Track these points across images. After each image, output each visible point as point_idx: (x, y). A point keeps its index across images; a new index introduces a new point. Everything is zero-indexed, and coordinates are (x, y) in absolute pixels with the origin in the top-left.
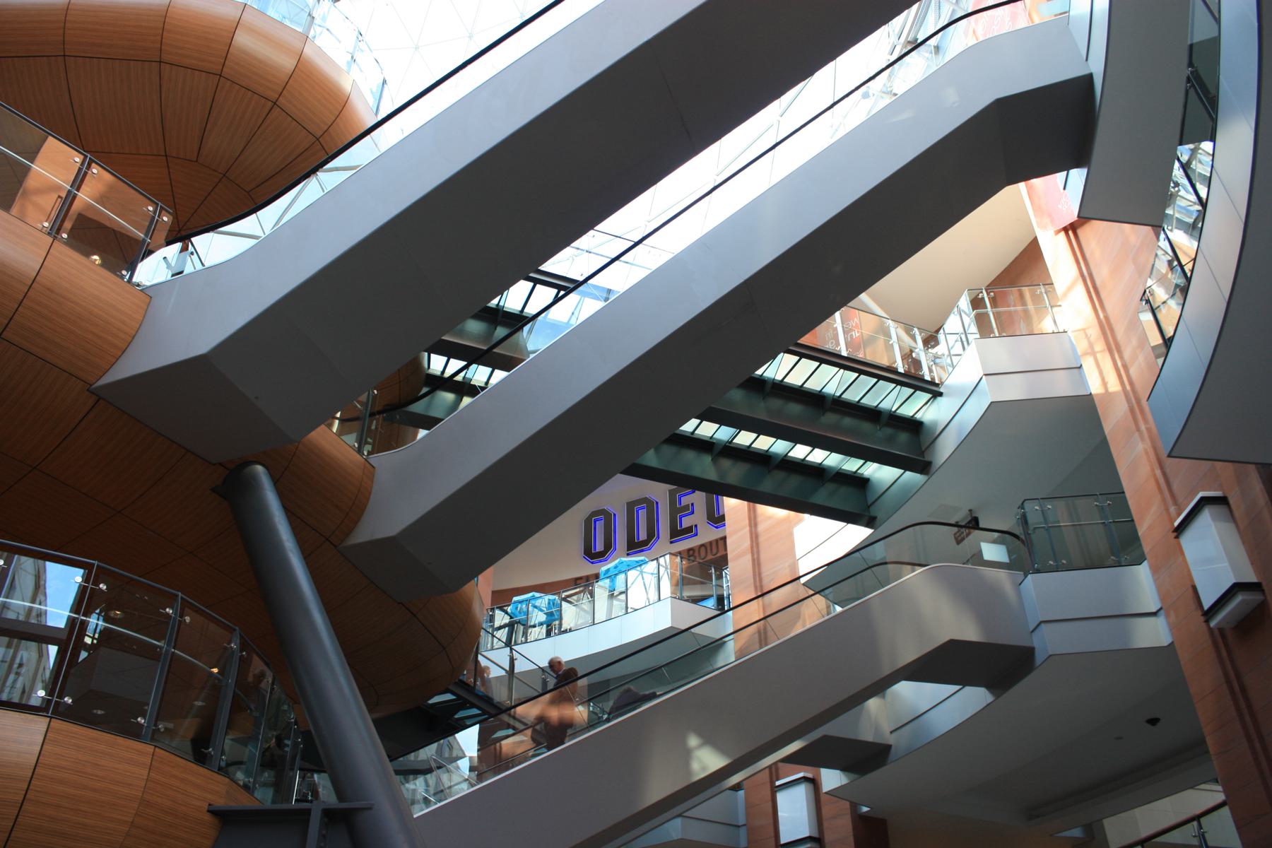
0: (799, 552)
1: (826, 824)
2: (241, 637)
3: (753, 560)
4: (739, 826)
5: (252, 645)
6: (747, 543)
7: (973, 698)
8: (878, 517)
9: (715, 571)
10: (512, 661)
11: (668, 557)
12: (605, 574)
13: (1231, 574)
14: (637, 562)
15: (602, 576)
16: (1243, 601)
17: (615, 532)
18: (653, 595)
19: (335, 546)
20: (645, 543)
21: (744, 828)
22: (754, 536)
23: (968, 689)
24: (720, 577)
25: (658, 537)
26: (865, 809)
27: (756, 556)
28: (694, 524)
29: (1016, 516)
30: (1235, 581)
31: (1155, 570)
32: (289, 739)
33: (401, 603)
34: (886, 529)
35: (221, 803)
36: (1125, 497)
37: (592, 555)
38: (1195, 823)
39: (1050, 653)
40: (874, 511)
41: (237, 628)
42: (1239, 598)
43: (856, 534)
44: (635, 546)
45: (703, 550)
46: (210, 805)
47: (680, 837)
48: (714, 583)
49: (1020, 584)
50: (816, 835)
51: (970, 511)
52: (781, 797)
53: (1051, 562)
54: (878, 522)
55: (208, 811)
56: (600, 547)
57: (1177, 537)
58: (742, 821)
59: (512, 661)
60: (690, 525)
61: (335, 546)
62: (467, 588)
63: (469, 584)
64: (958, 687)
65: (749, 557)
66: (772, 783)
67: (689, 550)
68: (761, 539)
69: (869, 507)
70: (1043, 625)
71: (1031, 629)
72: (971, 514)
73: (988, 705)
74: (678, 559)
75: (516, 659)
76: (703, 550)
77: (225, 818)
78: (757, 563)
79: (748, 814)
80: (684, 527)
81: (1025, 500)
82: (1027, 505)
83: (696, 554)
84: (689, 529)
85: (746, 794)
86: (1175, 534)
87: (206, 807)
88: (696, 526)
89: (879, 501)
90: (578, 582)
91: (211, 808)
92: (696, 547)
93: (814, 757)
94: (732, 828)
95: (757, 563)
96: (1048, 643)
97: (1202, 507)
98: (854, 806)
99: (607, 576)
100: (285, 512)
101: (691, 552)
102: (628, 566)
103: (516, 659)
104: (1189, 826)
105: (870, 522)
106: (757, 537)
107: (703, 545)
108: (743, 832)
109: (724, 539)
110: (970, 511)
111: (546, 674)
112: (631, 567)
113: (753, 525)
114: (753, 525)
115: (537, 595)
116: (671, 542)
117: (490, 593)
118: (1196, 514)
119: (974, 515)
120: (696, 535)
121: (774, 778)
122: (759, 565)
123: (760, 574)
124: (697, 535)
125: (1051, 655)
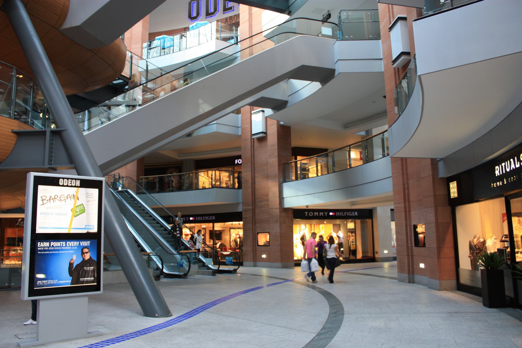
0: (263, 24)
1: (268, 127)
2: (16, 70)
3: (249, 24)
4: (239, 127)
5: (23, 73)
6: (247, 17)
7: (314, 86)
8: (292, 12)
9: (235, 28)
10: (147, 66)
11: (215, 22)
12: (192, 28)
13: (402, 48)
14: (205, 23)
15: (190, 29)
16: (403, 59)
17: (201, 9)
18: (209, 39)
19: (57, 29)
20: (213, 14)
21: (241, 128)
22: (250, 14)
23: (314, 83)
24: (237, 30)
25: (218, 11)
26: (282, 123)
27: (250, 23)
28: (233, 6)
29: (337, 16)
30: (402, 51)
31: (383, 43)
32: (45, 104)
33: (89, 50)
34: (294, 16)
35: (16, 129)
36: (378, 12)
37: (192, 18)
38: (382, 134)
39: (340, 72)
40: (291, 9)
41: (14, 67)
42: (403, 58)
43: (283, 17)
44: (209, 14)
45: (236, 17)
46: (12, 130)
47: (215, 131)
48: (234, 33)
49: (334, 44)
50: (265, 131)
51: (328, 11)
52: (253, 116)
53: (347, 37)
54: (292, 13)
55: (12, 132)
56: (195, 14)
57: (390, 31)
58: (240, 125)
59: (147, 66)
60: (231, 6)
61: (57, 29)
62: (117, 41)
63: (117, 39)
64: (311, 82)
65: (248, 23)
66: (251, 112)
67: (230, 17)
68: (253, 16)
69: (289, 7)
70: (339, 61)
71: (335, 62)
72: (328, 12)
73: (320, 89)
74: (220, 23)
75: (149, 65)
76: (236, 17)
77: (18, 134)
78: (251, 26)
79: (242, 124)
80: (229, 7)
81: (341, 11)
82: (342, 12)
83: (233, 19)
84: (231, 8)
85: (242, 116)
86: (389, 30)
87: (11, 131)
88: (234, 7)
89: (293, 4)
90: (186, 29)
91: (13, 131)
92: (233, 16)
93: (262, 103)
94: (237, 128)
95: (251, 26)
96: (340, 68)
97: (398, 21)
98: (278, 122)
99: (193, 29)
100: (29, 15)
101: (231, 18)
102: (201, 25)
103: (149, 65)
104: (380, 135)
105: (289, 13)
106: (251, 14)
107: (235, 15)
108: (240, 129)
109: (239, 14)
110: (328, 11)
111: (162, 71)
112: (202, 25)
113: (250, 10)
114: (250, 10)
115: (165, 36)
116: (224, 13)
117: (148, 35)
118: (396, 23)
119: (330, 13)
120: (233, 10)
121: (252, 110)
122: (251, 26)
123: (251, 30)
124: (234, 10)
125: (339, 73)
